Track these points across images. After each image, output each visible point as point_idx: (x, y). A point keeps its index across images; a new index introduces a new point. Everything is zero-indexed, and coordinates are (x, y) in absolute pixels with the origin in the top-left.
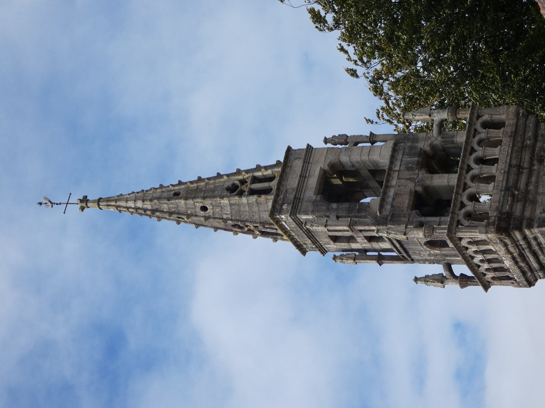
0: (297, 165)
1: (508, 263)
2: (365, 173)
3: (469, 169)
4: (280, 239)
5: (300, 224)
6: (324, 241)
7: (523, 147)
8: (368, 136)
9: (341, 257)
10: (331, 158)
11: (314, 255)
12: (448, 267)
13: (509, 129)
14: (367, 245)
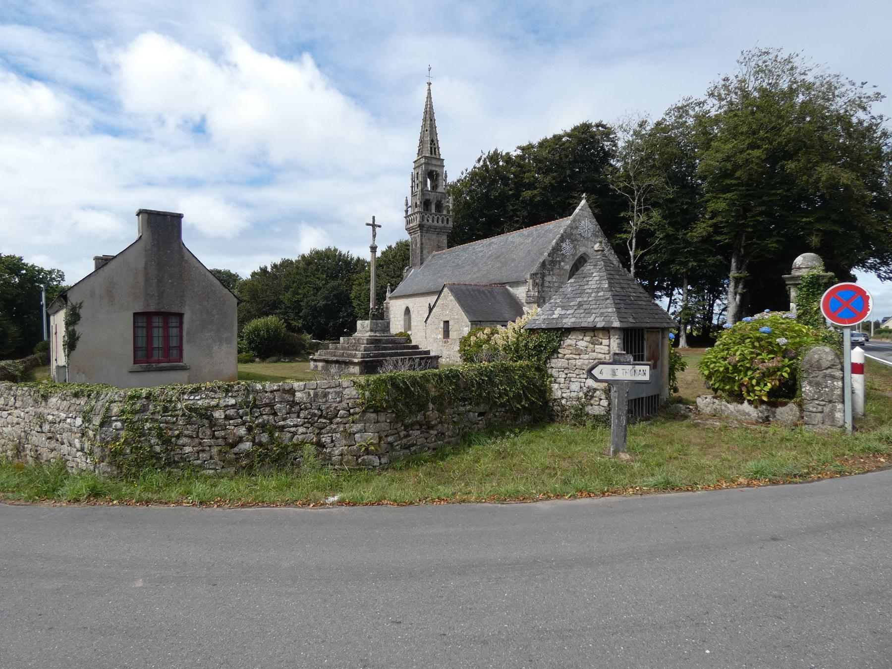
0: (439, 163)
1: (411, 225)
2: (436, 183)
5: (421, 165)
8: (411, 341)
9: (412, 175)
10: (440, 174)
11: (413, 165)
13: (446, 225)
14: (416, 183)
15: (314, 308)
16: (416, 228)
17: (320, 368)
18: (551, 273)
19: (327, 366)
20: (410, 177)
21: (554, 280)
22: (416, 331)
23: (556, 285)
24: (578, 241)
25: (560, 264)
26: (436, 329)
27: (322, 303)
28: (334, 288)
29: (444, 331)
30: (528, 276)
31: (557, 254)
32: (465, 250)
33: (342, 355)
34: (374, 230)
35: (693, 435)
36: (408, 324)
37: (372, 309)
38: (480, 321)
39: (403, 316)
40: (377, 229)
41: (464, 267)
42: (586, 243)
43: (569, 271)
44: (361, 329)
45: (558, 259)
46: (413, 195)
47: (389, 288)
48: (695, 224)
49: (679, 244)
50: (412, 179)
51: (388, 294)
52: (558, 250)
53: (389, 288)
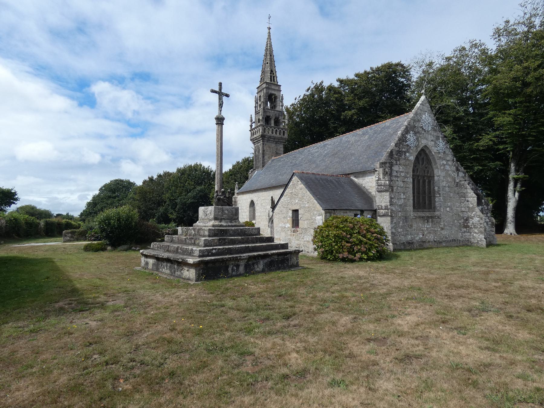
0: (277, 88)
1: (255, 136)
2: (275, 104)
5: (263, 89)
6: (260, 94)
7: (279, 140)
9: (256, 98)
10: (278, 97)
11: (256, 91)
12: (254, 122)
13: (283, 137)
14: (259, 104)
15: (184, 204)
16: (259, 138)
17: (150, 266)
18: (398, 163)
19: (158, 265)
20: (254, 100)
21: (401, 170)
22: (260, 220)
23: (403, 174)
24: (420, 134)
25: (405, 155)
26: (284, 218)
27: (190, 201)
28: (200, 191)
29: (293, 221)
30: (378, 165)
31: (403, 145)
32: (301, 153)
33: (176, 251)
34: (220, 99)
36: (253, 215)
37: (217, 192)
38: (334, 210)
39: (248, 208)
40: (224, 98)
41: (302, 165)
42: (427, 136)
43: (413, 161)
44: (203, 217)
45: (404, 150)
46: (257, 113)
47: (236, 186)
48: (480, 135)
49: (466, 152)
50: (256, 101)
51: (236, 191)
52: (403, 141)
53: (236, 186)
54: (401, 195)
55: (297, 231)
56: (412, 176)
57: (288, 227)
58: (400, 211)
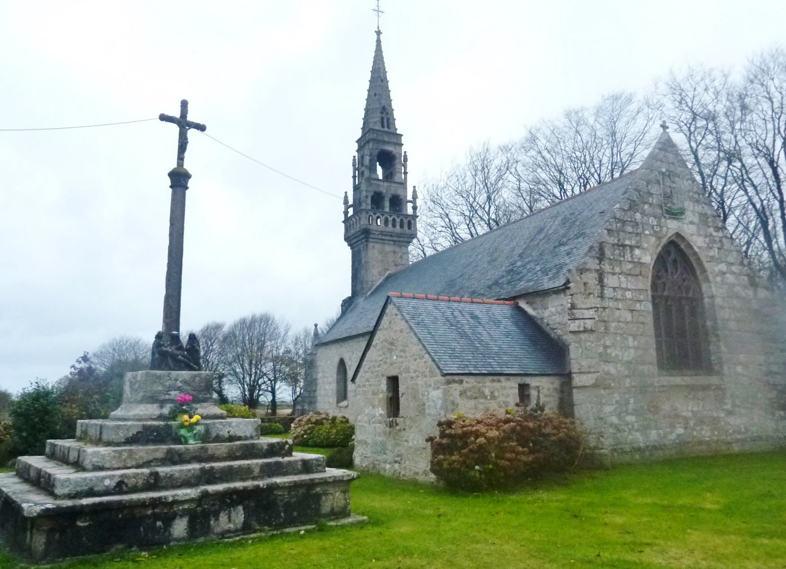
0: (394, 140)
3: (391, 216)
4: (773, 399)
21: (624, 286)
35: (404, 375)
40: (192, 133)
54: (626, 339)
55: (397, 424)
56: (650, 297)
57: (381, 415)
58: (626, 376)
